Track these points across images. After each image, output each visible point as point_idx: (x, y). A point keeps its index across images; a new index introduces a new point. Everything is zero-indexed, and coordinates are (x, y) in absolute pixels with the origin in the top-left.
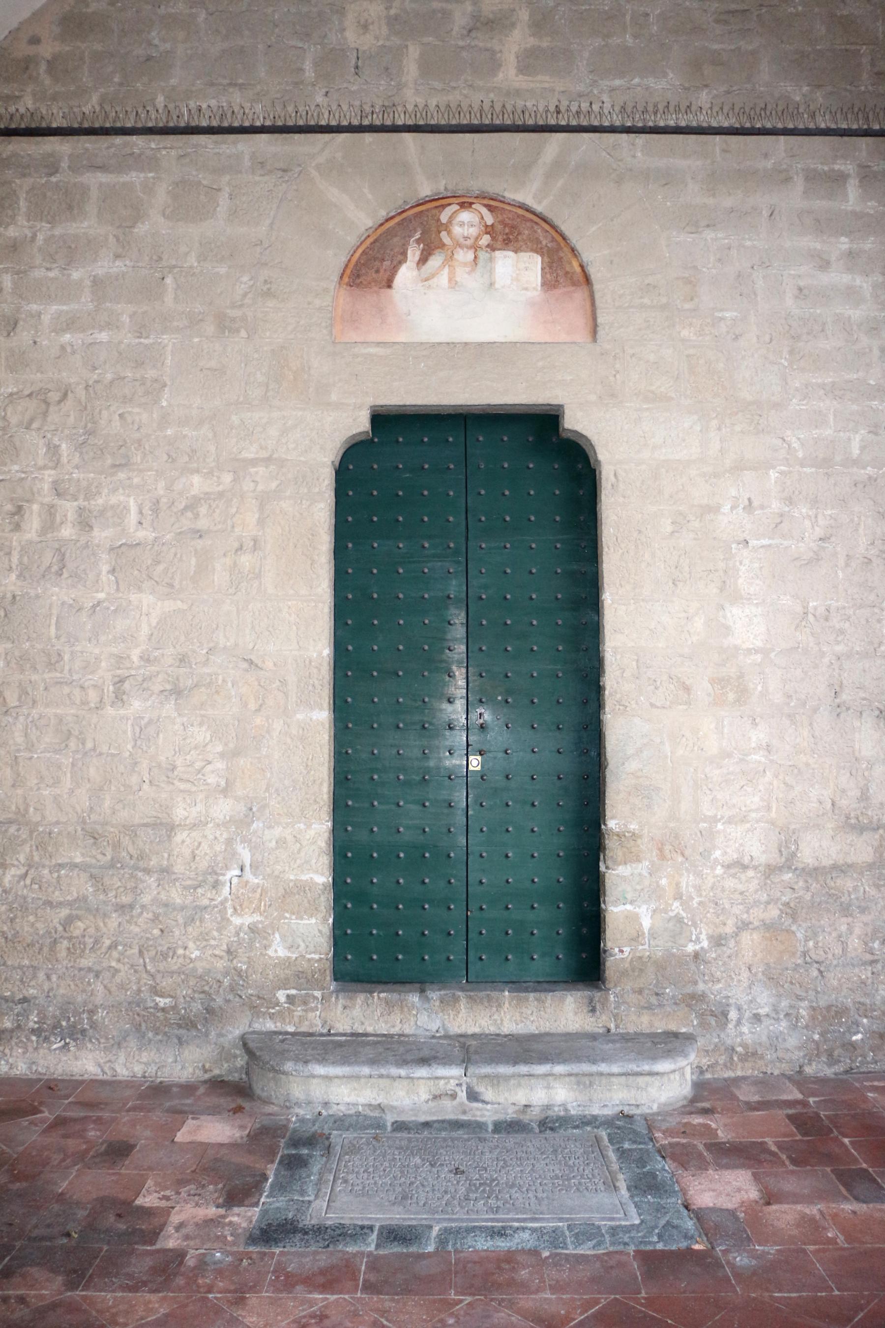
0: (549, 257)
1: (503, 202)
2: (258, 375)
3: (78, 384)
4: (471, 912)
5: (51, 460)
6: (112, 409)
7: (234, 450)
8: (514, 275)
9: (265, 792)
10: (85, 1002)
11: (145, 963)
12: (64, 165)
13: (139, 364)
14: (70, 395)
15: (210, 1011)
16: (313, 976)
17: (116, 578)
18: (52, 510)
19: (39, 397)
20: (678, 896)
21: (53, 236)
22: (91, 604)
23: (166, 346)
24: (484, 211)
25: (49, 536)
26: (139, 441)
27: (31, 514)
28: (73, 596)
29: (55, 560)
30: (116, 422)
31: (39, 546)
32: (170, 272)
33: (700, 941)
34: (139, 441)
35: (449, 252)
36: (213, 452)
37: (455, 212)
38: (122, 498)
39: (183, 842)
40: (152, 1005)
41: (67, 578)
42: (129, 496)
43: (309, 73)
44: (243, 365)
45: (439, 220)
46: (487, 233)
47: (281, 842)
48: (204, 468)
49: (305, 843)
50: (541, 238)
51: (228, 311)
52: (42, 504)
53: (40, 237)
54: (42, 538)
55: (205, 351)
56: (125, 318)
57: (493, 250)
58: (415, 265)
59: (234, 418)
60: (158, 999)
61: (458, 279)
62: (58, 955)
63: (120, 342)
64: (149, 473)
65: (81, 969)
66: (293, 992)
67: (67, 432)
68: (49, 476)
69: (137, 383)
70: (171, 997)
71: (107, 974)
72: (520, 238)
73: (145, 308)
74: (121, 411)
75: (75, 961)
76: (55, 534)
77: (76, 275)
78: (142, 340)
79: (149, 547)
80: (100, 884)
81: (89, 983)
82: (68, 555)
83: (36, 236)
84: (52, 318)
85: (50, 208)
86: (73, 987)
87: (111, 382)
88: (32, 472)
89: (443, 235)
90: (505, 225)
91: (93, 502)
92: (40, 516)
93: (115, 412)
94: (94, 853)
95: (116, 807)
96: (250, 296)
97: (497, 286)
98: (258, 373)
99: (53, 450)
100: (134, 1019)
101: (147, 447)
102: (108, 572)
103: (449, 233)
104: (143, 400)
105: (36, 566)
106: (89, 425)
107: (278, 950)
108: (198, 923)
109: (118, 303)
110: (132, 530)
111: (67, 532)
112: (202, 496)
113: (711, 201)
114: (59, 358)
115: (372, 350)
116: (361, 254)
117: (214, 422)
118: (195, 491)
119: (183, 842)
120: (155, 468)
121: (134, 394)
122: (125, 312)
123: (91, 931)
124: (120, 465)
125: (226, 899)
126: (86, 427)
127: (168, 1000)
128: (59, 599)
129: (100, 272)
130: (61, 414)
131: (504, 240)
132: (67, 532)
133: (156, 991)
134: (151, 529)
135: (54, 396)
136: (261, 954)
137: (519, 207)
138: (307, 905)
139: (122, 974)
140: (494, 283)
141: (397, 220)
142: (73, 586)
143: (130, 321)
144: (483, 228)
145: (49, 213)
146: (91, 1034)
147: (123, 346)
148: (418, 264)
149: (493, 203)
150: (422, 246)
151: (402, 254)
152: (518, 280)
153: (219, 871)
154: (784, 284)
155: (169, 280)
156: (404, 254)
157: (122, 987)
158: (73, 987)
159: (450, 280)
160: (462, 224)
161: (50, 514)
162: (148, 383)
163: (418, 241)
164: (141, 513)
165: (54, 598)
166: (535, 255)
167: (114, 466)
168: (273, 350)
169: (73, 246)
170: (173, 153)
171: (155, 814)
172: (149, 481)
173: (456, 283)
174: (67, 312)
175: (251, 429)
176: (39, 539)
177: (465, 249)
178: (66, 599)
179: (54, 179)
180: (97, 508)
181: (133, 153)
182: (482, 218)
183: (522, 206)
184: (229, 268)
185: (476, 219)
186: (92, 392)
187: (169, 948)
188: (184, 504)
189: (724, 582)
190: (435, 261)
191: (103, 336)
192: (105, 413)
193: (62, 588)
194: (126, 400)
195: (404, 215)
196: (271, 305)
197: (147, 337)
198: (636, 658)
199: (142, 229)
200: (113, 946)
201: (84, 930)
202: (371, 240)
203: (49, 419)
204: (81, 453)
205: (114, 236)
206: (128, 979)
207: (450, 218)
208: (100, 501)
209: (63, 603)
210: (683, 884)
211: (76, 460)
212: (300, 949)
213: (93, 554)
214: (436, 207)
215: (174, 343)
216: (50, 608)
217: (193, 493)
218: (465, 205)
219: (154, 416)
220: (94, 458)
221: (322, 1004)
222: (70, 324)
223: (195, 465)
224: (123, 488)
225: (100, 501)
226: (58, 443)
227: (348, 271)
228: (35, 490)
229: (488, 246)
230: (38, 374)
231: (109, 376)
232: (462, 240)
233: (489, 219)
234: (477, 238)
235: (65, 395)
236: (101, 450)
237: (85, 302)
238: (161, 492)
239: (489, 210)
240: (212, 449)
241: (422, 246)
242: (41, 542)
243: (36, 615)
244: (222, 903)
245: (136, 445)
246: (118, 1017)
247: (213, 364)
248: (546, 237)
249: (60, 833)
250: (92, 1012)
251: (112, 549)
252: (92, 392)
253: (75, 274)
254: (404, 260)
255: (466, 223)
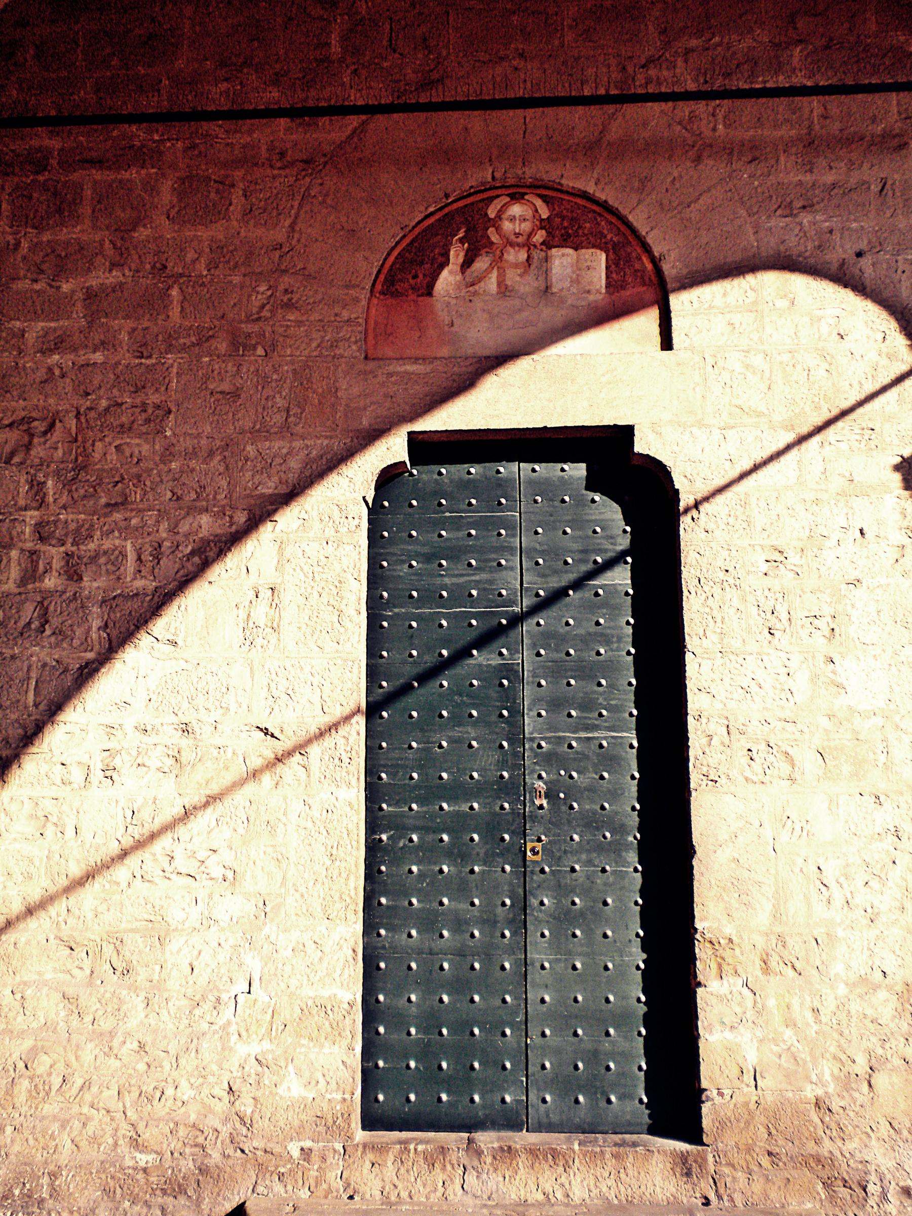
0: (614, 253)
1: (561, 191)
2: (278, 399)
3: (67, 412)
4: (531, 1039)
5: (34, 499)
6: (107, 440)
7: (250, 485)
8: (574, 276)
9: (280, 887)
10: (46, 1162)
11: (124, 1107)
12: (54, 162)
13: (138, 389)
14: (58, 424)
15: (203, 1170)
16: (334, 1122)
17: (108, 635)
18: (34, 557)
19: (21, 427)
20: (790, 1023)
21: (41, 243)
22: (78, 666)
23: (172, 366)
24: (539, 203)
25: (30, 586)
26: (139, 477)
27: (9, 561)
28: (56, 657)
29: (36, 614)
30: (113, 456)
31: (18, 598)
32: (175, 282)
33: (823, 1080)
34: (139, 477)
35: (498, 252)
36: (225, 488)
37: (506, 204)
38: (117, 542)
39: (179, 951)
40: (131, 1163)
41: (50, 636)
42: (125, 539)
43: (336, 48)
44: (260, 388)
45: (486, 214)
46: (541, 229)
47: (299, 949)
48: (214, 506)
49: (327, 950)
50: (606, 232)
51: (243, 326)
52: (22, 550)
53: (25, 244)
54: (22, 590)
55: (216, 372)
56: (124, 336)
57: (550, 247)
58: (459, 269)
59: (249, 448)
60: (138, 1156)
61: (509, 283)
62: (16, 1100)
63: (118, 363)
64: (150, 513)
65: (43, 1118)
66: (308, 1144)
67: (53, 466)
68: (31, 517)
69: (138, 410)
70: (157, 1152)
71: (77, 1125)
72: (580, 232)
73: (146, 324)
74: (118, 442)
75: (36, 1108)
76: (37, 584)
77: (66, 287)
78: (143, 361)
79: (148, 598)
80: (74, 1008)
81: (53, 1137)
82: (52, 608)
83: (20, 242)
84: (38, 337)
85: (37, 211)
86: (31, 1142)
87: (107, 409)
88: (11, 514)
89: (491, 231)
90: (563, 218)
91: (83, 547)
92: (20, 565)
93: (110, 444)
94: (69, 966)
95: (100, 909)
96: (267, 307)
97: (554, 290)
98: (277, 396)
99: (37, 487)
100: (107, 1183)
101: (148, 483)
102: (99, 629)
103: (498, 229)
104: (144, 429)
105: (13, 621)
106: (80, 459)
107: (292, 1089)
108: (193, 1054)
109: (114, 319)
110: (128, 579)
111: (50, 582)
112: (212, 538)
113: (808, 178)
114: (46, 381)
115: (410, 368)
116: (396, 258)
117: (226, 453)
118: (204, 533)
119: (179, 951)
120: (157, 507)
121: (133, 422)
122: (122, 328)
123: (60, 1066)
124: (116, 504)
125: (229, 1023)
126: (76, 460)
127: (151, 1157)
128: (39, 661)
129: (93, 283)
130: (47, 446)
131: (562, 235)
132: (50, 582)
133: (136, 1143)
134: (152, 578)
135: (39, 426)
136: (271, 1092)
137: (579, 196)
138: (329, 1029)
139: (95, 1122)
140: (551, 286)
141: (437, 217)
142: (57, 645)
143: (130, 338)
144: (538, 223)
145: (35, 217)
146: (51, 1206)
147: (120, 367)
148: (461, 269)
149: (548, 191)
150: (466, 245)
151: (442, 255)
152: (578, 281)
153: (222, 988)
154: (899, 272)
155: (175, 292)
156: (446, 255)
157: (94, 1140)
158: (31, 1142)
159: (499, 284)
160: (512, 219)
161: (32, 561)
162: (150, 411)
163: (461, 241)
164: (139, 559)
165: (34, 659)
166: (598, 251)
167: (108, 505)
168: (295, 370)
169: (63, 254)
170: (179, 145)
171: (147, 917)
172: (149, 522)
173: (506, 287)
174: (55, 330)
175: (269, 461)
176: (17, 591)
177: (517, 248)
178: (48, 659)
179: (41, 178)
180: (88, 554)
181: (134, 145)
182: (537, 211)
183: (584, 195)
184: (244, 275)
185: (529, 213)
186: (83, 420)
187: (155, 1088)
188: (190, 548)
189: (833, 629)
190: (481, 264)
191: (98, 357)
192: (99, 445)
193: (43, 647)
194: (124, 429)
195: (446, 210)
196: (292, 318)
197: (150, 357)
198: (727, 723)
199: (142, 233)
200: (86, 1085)
201: (51, 1067)
202: (407, 240)
203: (33, 452)
204: (70, 491)
205: (110, 241)
206: (103, 1130)
207: (499, 211)
208: (92, 546)
209: (45, 665)
210: (796, 1006)
211: (65, 499)
212: (320, 1086)
213: (82, 607)
214: (483, 200)
215: (180, 363)
216: (28, 670)
217: (201, 535)
218: (517, 197)
219: (157, 447)
220: (85, 496)
221: (344, 1160)
222: (58, 344)
223: (204, 503)
224: (119, 531)
225: (92, 546)
226: (43, 480)
227: (382, 277)
228: (14, 533)
229: (542, 243)
230: (21, 401)
231: (104, 403)
232: (513, 237)
233: (544, 213)
234: (530, 235)
235: (52, 426)
236: (94, 487)
237: (77, 319)
238: (164, 535)
239: (544, 201)
240: (224, 483)
241: (466, 245)
242: (20, 594)
243: (12, 680)
244: (224, 1028)
245: (135, 481)
246: (87, 1181)
247: (226, 386)
248: (610, 231)
249: (28, 943)
250: (53, 1176)
251: (104, 602)
252: (83, 420)
253: (64, 286)
254: (447, 262)
255: (518, 217)
